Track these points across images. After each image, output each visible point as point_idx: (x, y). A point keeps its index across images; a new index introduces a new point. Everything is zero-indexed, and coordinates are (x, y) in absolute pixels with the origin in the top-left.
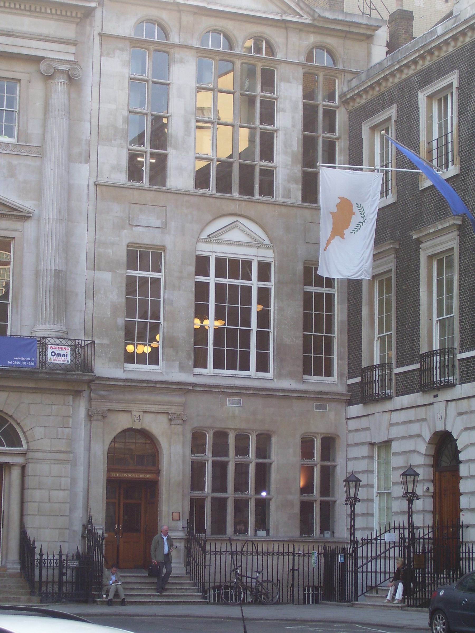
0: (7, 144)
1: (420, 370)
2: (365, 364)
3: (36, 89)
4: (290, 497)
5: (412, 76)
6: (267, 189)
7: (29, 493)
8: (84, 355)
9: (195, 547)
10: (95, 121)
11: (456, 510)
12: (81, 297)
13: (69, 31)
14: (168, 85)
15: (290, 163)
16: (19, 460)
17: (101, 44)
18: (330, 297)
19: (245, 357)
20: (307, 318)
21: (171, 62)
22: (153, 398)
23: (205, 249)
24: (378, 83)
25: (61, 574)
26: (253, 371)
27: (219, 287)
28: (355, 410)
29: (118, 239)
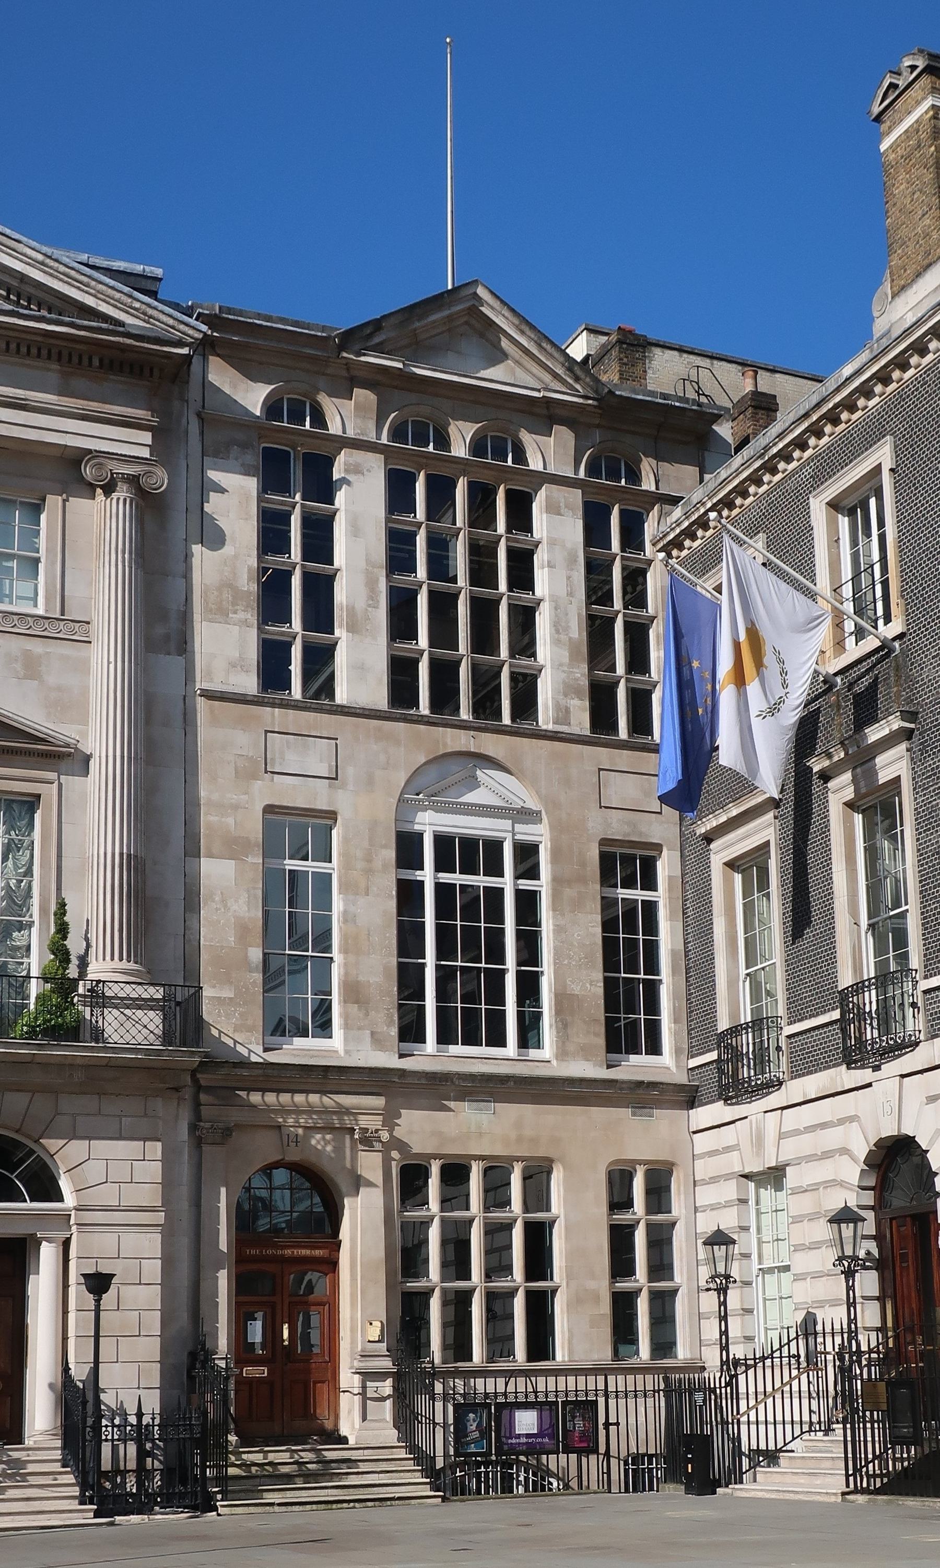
2: (723, 1024)
4: (592, 1285)
5: (795, 472)
15: (566, 660)
17: (202, 433)
18: (650, 908)
19: (497, 1019)
20: (609, 946)
27: (443, 891)
29: (245, 797)
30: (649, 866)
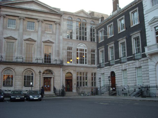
0: (51, 33)
1: (99, 66)
2: (100, 63)
3: (55, 26)
4: (90, 81)
6: (86, 40)
7: (55, 81)
8: (62, 62)
9: (78, 88)
10: (62, 30)
11: (115, 82)
12: (61, 54)
13: (59, 18)
14: (72, 25)
16: (53, 77)
20: (92, 57)
21: (73, 22)
22: (71, 68)
23: (78, 48)
24: (101, 25)
25: (60, 92)
26: (85, 64)
27: (80, 53)
28: (99, 69)
30: (95, 51)
